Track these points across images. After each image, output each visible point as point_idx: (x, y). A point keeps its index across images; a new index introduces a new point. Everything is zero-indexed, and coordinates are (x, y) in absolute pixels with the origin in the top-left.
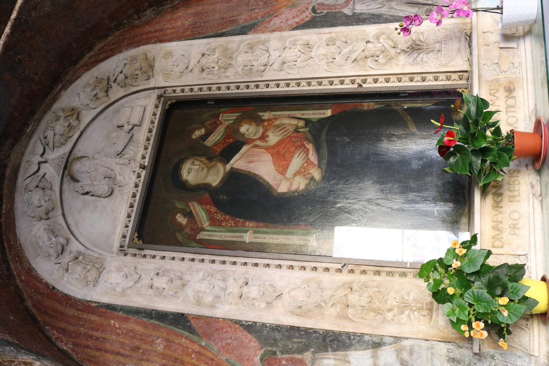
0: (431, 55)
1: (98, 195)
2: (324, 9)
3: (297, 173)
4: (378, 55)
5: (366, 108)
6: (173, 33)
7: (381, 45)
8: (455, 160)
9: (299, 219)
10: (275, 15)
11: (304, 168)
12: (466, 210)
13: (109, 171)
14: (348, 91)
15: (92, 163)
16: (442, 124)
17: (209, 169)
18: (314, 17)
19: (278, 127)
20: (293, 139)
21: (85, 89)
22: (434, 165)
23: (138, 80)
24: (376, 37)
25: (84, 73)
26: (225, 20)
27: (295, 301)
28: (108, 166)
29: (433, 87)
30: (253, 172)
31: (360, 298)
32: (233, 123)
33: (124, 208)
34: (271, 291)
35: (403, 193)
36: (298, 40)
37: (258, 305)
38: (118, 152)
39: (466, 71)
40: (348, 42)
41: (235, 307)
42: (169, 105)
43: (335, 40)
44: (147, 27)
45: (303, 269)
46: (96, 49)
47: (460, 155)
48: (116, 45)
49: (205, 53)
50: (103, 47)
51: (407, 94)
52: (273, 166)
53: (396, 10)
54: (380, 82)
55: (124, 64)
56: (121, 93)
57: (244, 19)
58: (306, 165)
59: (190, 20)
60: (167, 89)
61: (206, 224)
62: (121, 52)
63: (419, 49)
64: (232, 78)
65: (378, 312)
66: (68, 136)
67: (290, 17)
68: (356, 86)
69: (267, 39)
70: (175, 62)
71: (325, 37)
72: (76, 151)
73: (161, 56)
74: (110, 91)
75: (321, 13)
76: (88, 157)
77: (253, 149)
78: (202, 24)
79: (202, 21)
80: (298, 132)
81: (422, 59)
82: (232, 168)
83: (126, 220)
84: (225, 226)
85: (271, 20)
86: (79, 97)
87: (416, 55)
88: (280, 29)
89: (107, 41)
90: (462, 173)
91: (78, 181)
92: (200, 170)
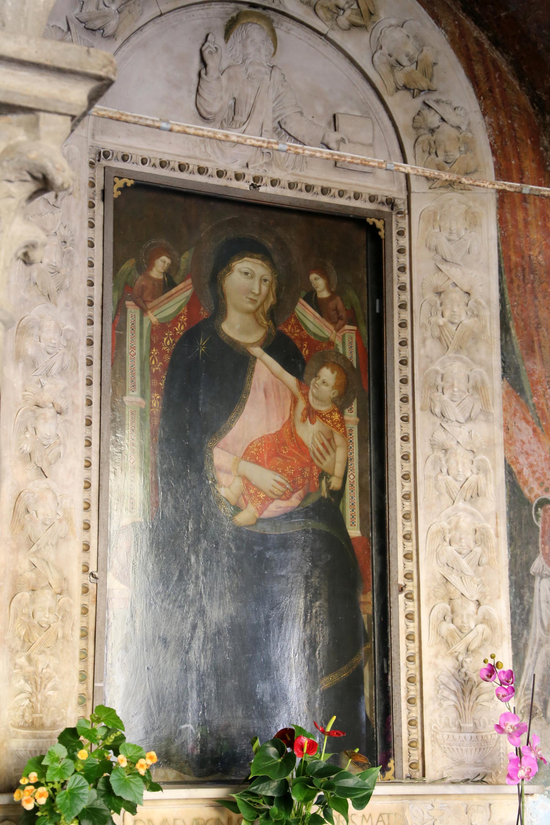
0: (452, 714)
1: (200, 90)
2: (544, 522)
3: (247, 482)
4: (455, 621)
5: (362, 598)
6: (516, 226)
7: (472, 626)
8: (272, 756)
9: (169, 490)
10: (539, 430)
11: (256, 494)
12: (187, 778)
13: (248, 109)
14: (392, 569)
15: (263, 69)
16: (329, 734)
17: (254, 313)
18: (529, 504)
19: (329, 440)
20: (307, 469)
21: (412, 39)
22: (263, 719)
23: (427, 155)
24: (487, 617)
25: (447, 31)
26: (534, 332)
27: (36, 501)
28: (258, 106)
29: (398, 718)
30: (249, 400)
31: (47, 610)
32: (338, 353)
33: (178, 151)
34: (50, 457)
35: (216, 670)
36: (486, 475)
37: (27, 438)
38: (285, 123)
39: (424, 775)
40: (481, 568)
41: (20, 397)
42: (374, 223)
43: (485, 544)
44: (534, 165)
45: (86, 506)
46: (496, 55)
47: (281, 763)
48: (500, 101)
49: (472, 296)
50: (498, 69)
51: (386, 671)
52: (260, 435)
53: (537, 653)
54: (408, 624)
55: (458, 124)
56: (400, 120)
57: (533, 370)
58: (262, 496)
59: (540, 258)
60: (407, 216)
61: (152, 317)
62: (484, 115)
63: (463, 693)
64: (422, 352)
65: (27, 640)
66: (318, 7)
67: (531, 459)
68: (401, 581)
69: (491, 418)
70: (458, 235)
71: (490, 527)
72: (287, 24)
73: (471, 204)
74: (407, 95)
75: (537, 516)
76: (274, 53)
77: (289, 395)
78: (529, 285)
79: (536, 284)
80: (320, 477)
81: (445, 698)
82: (255, 358)
83: (156, 158)
84: (151, 355)
85: (528, 422)
86: (398, 26)
87: (453, 688)
88: (509, 441)
89: (510, 77)
90: (252, 766)
91: (227, 36)
92: (251, 296)
